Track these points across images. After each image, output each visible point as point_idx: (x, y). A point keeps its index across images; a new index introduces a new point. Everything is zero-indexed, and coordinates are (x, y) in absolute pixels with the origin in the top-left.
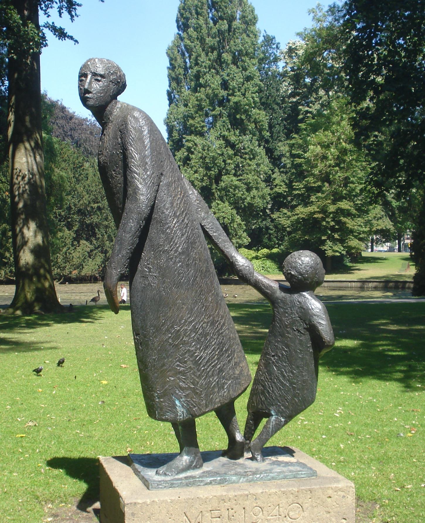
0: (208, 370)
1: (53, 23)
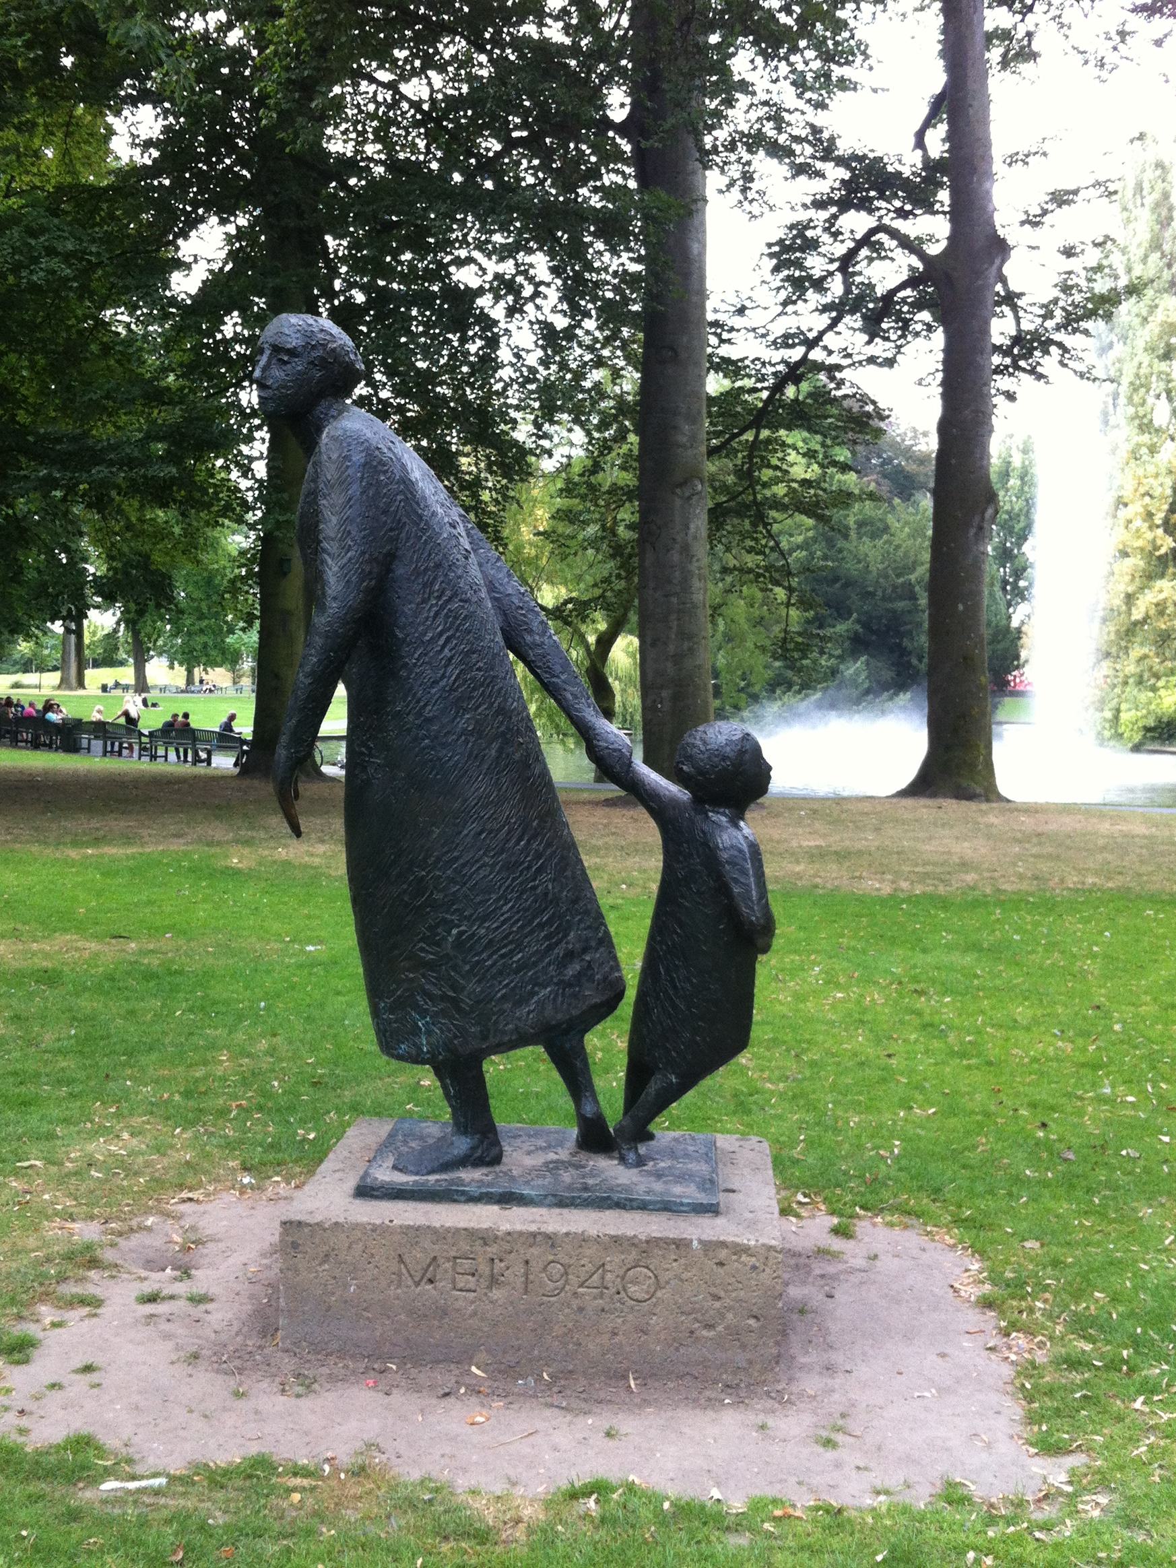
0: (489, 963)
1: (172, 667)
